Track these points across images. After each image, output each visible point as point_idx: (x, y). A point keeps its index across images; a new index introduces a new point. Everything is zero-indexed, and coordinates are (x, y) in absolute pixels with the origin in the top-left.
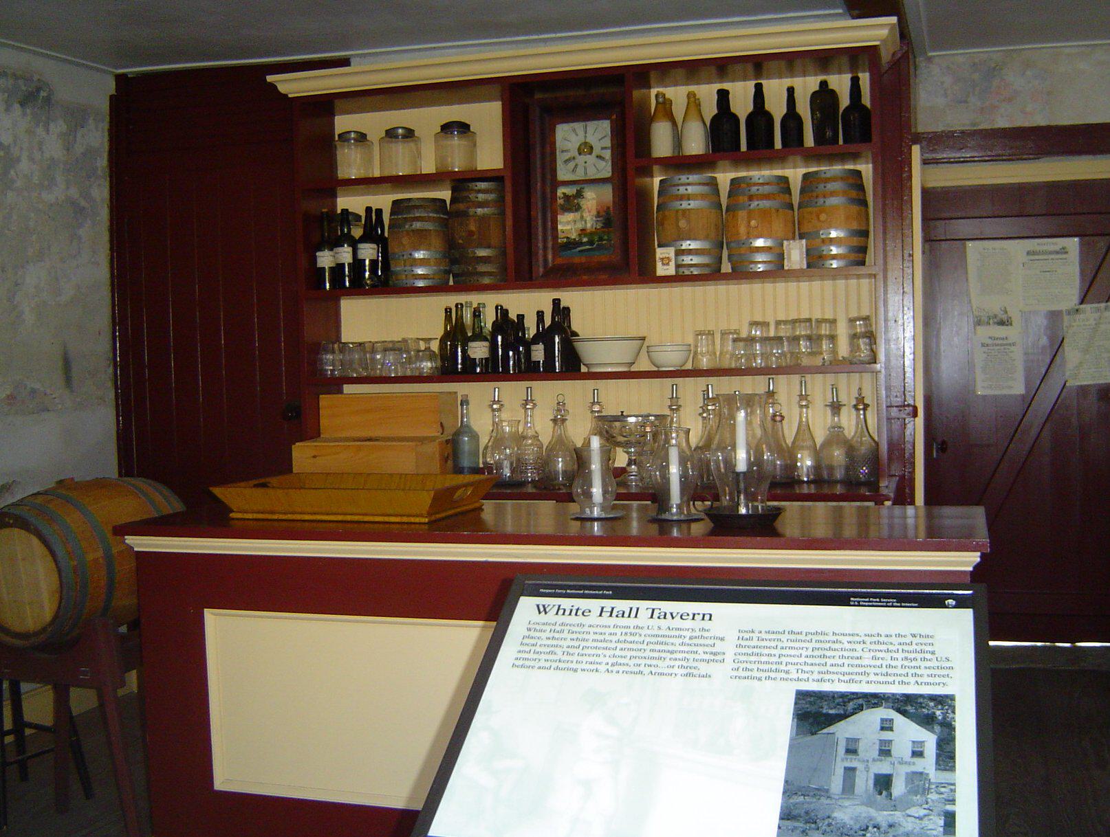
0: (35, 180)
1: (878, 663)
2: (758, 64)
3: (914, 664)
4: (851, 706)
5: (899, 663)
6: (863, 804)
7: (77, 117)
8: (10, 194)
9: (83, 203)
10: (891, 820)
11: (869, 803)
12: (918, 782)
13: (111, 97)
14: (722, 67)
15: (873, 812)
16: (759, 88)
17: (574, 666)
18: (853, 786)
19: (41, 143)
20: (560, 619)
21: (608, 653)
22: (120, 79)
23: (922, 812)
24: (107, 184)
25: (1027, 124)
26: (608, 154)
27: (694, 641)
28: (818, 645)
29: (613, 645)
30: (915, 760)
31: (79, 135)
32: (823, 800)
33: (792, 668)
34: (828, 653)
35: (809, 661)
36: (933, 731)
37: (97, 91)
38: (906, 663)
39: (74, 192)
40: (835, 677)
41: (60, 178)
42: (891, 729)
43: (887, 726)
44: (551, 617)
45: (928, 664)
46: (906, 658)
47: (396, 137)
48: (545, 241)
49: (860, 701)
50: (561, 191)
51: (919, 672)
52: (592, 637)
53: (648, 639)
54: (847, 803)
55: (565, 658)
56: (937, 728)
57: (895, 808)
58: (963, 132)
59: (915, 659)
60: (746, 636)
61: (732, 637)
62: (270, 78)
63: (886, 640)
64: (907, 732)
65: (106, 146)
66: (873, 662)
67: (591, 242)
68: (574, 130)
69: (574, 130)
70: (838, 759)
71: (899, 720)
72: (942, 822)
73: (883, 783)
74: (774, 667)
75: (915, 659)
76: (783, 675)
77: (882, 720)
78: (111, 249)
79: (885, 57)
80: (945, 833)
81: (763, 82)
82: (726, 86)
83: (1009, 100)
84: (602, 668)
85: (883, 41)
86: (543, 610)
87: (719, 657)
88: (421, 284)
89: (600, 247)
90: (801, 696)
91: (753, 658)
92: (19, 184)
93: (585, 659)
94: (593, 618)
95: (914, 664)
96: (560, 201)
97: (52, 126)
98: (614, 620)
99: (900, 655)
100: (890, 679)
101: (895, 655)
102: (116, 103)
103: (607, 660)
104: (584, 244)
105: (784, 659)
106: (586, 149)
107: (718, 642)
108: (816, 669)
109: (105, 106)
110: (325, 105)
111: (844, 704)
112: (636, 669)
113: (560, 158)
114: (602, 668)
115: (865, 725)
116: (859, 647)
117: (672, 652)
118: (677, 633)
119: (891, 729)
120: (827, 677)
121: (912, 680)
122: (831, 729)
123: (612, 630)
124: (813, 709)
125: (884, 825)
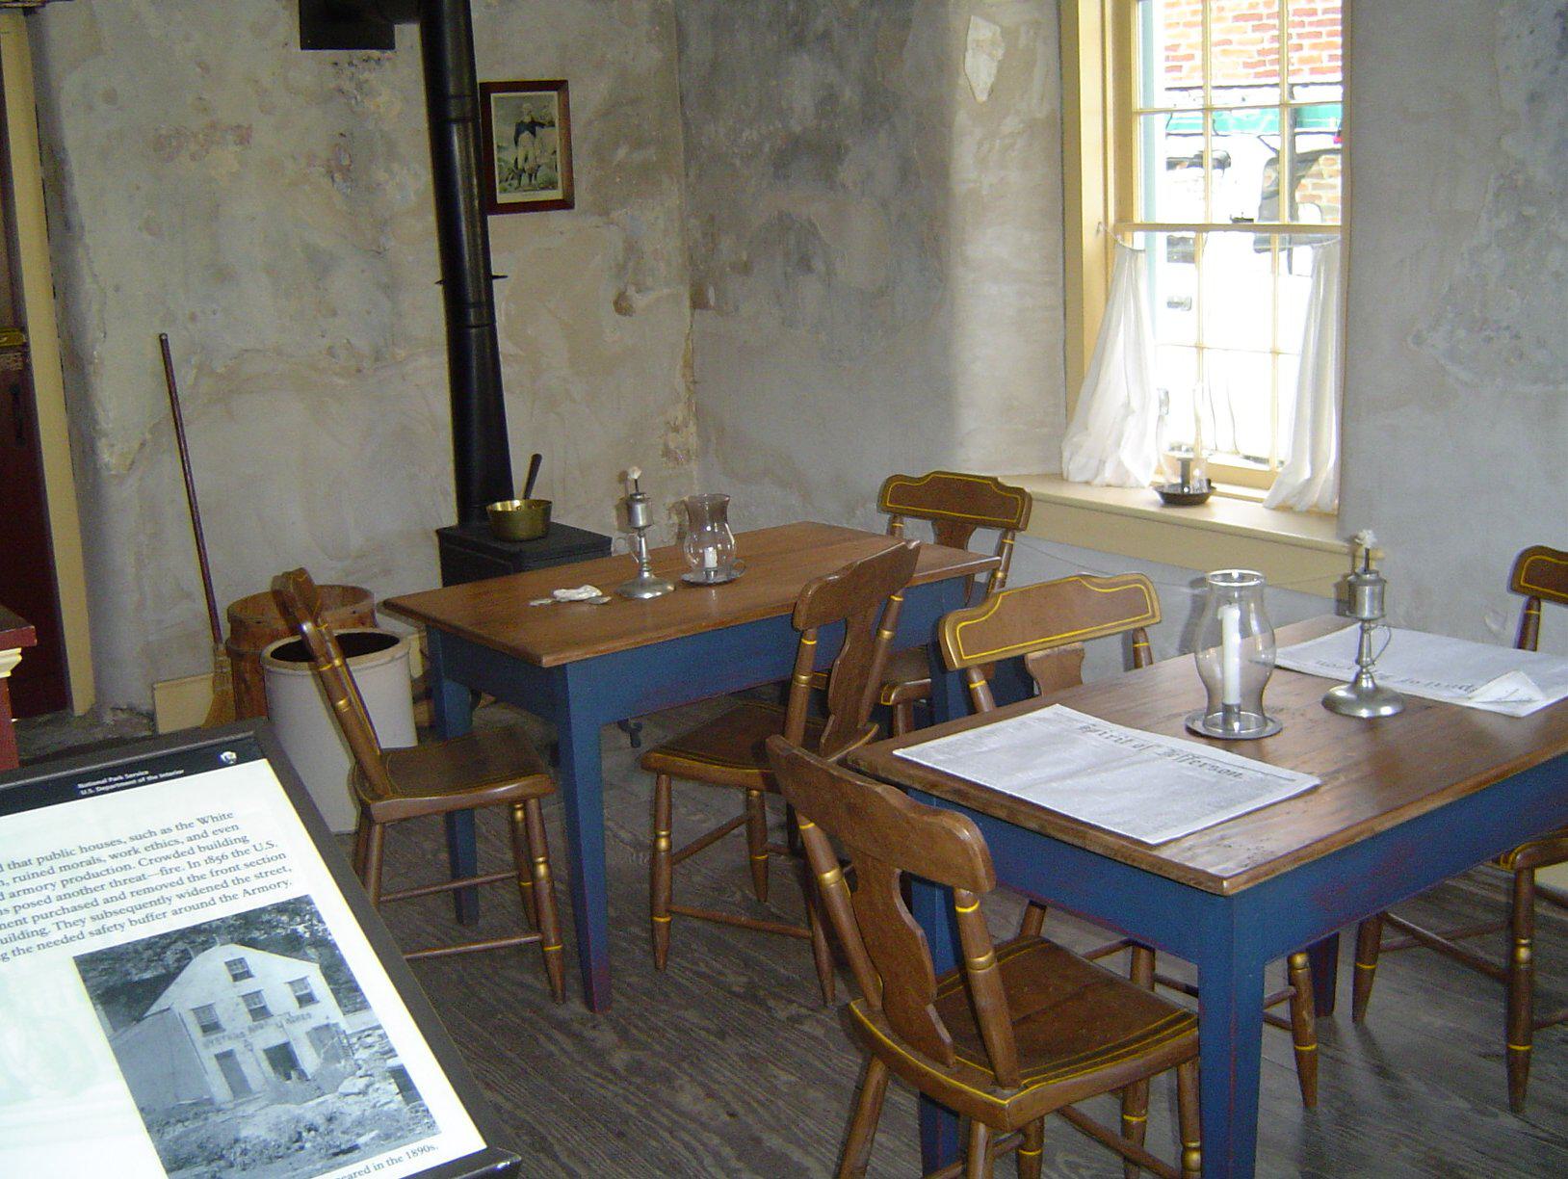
4: (170, 957)
10: (327, 1110)
11: (282, 1097)
15: (294, 1109)
23: (361, 1083)
34: (91, 883)
35: (68, 903)
36: (306, 958)
42: (247, 974)
49: (180, 945)
54: (250, 1109)
56: (311, 952)
64: (276, 973)
71: (253, 957)
72: (394, 1088)
76: (39, 940)
111: (159, 957)
116: (132, 860)
120: (109, 922)
121: (238, 890)
125: (320, 1121)
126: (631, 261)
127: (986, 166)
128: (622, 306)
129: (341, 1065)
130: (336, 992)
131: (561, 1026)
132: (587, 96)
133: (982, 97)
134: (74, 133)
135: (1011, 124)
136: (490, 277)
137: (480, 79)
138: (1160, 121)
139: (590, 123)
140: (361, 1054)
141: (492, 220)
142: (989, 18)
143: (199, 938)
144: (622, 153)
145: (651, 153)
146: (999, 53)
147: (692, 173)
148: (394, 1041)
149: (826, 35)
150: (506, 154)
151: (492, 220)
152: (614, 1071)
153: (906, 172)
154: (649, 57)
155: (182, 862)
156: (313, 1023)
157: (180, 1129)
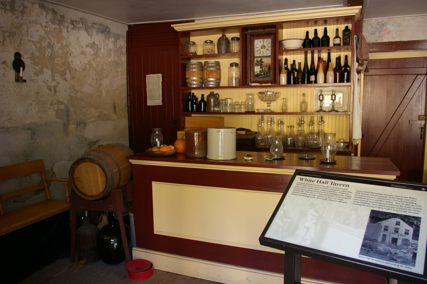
0: (106, 55)
1: (398, 205)
2: (325, 21)
3: (409, 206)
4: (387, 216)
5: (404, 206)
6: (387, 246)
7: (117, 37)
8: (98, 59)
9: (119, 62)
10: (395, 252)
11: (389, 246)
12: (406, 242)
13: (127, 31)
14: (316, 22)
15: (390, 249)
16: (326, 29)
17: (308, 196)
18: (385, 240)
19: (107, 44)
20: (306, 182)
21: (318, 193)
22: (129, 26)
23: (406, 251)
24: (126, 56)
25: (393, 41)
26: (270, 49)
27: (343, 192)
28: (380, 197)
29: (320, 191)
30: (406, 235)
31: (118, 42)
32: (375, 243)
33: (371, 203)
34: (382, 200)
35: (376, 202)
36: (412, 227)
37: (123, 30)
38: (407, 206)
39: (116, 58)
40: (384, 207)
41: (112, 54)
42: (399, 225)
43: (398, 224)
44: (303, 181)
45: (414, 207)
46: (407, 204)
47: (208, 43)
48: (251, 74)
49: (390, 215)
50: (255, 60)
51: (410, 209)
52: (314, 188)
53: (330, 190)
54: (382, 245)
55: (306, 193)
56: (414, 227)
57: (397, 249)
58: (373, 43)
59: (410, 205)
60: (358, 192)
61: (354, 192)
62: (172, 26)
63: (401, 198)
64: (404, 226)
65: (126, 46)
66: (396, 204)
67: (264, 75)
68: (260, 41)
69: (260, 41)
70: (381, 232)
71: (402, 222)
72: (412, 255)
73: (395, 241)
74: (365, 202)
75: (410, 205)
76: (368, 205)
77: (397, 222)
78: (127, 75)
79: (356, 19)
80: (413, 259)
81: (328, 27)
82: (316, 28)
83: (388, 33)
84: (316, 197)
85: (357, 14)
86: (302, 179)
87: (349, 198)
88: (194, 86)
89: (267, 76)
90: (373, 211)
91: (359, 199)
92: (101, 56)
93: (311, 194)
94: (315, 183)
95: (409, 206)
96: (255, 62)
97: (110, 39)
98: (321, 184)
99: (405, 203)
100: (401, 210)
101: (403, 203)
102: (128, 32)
103: (317, 195)
104: (262, 75)
105: (369, 200)
106: (263, 47)
107: (350, 193)
108: (378, 204)
109: (125, 34)
110: (187, 34)
111: (386, 215)
112: (325, 198)
113: (256, 49)
114: (316, 197)
115: (391, 223)
116: (392, 199)
117: (336, 195)
118: (338, 189)
119: (399, 225)
120: (381, 207)
121: (408, 211)
122: (380, 222)
123: (320, 187)
124: (376, 216)
125: (393, 253)
129: (405, 247)
148: (419, 248)
157: (369, 241)
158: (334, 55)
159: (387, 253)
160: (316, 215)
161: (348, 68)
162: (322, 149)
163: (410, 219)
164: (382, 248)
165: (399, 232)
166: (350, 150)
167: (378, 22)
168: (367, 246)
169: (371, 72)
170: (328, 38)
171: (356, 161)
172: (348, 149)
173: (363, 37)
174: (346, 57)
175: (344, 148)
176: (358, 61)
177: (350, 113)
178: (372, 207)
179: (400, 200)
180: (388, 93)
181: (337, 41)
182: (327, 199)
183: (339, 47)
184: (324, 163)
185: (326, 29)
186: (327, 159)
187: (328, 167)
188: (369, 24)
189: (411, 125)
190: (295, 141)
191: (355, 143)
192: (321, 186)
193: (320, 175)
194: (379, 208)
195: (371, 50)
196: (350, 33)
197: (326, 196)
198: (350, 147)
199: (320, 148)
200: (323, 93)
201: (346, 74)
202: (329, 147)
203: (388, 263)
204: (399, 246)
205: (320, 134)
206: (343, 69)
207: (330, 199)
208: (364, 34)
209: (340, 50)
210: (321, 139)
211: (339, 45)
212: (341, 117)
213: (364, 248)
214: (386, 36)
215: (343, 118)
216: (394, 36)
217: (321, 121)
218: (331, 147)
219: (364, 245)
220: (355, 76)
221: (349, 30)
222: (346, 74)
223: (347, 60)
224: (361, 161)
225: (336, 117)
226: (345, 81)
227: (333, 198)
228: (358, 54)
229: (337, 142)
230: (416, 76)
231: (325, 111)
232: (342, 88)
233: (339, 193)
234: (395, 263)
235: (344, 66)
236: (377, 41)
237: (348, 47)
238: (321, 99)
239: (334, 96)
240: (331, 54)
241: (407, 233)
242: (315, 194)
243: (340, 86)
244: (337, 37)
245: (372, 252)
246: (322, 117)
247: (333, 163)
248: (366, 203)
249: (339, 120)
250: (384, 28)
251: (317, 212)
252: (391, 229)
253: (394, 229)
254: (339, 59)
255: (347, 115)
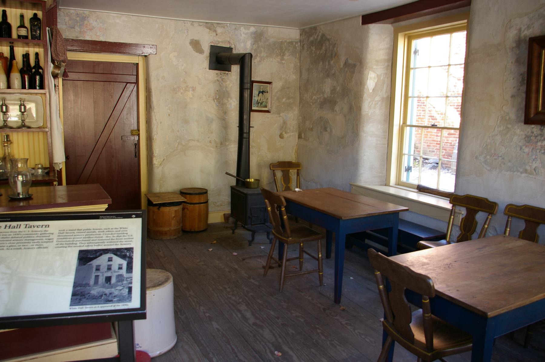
4: (98, 254)
6: (101, 287)
10: (110, 292)
11: (103, 287)
12: (120, 278)
15: (104, 290)
23: (121, 288)
25: (97, 40)
29: (10, 239)
33: (78, 242)
34: (91, 236)
35: (84, 239)
36: (125, 260)
40: (93, 244)
42: (111, 261)
45: (125, 237)
49: (101, 252)
53: (24, 236)
54: (95, 288)
56: (127, 259)
57: (112, 287)
58: (73, 40)
60: (62, 232)
61: (56, 232)
64: (117, 261)
71: (115, 258)
72: (127, 290)
76: (75, 245)
83: (91, 30)
91: (64, 240)
98: (11, 230)
103: (6, 245)
105: (75, 240)
107: (51, 235)
111: (96, 253)
112: (19, 247)
114: (5, 248)
115: (103, 260)
116: (102, 233)
117: (33, 240)
119: (111, 261)
120: (90, 244)
121: (119, 243)
125: (108, 293)
126: (284, 127)
127: (371, 108)
128: (281, 136)
129: (120, 283)
130: (127, 268)
131: (239, 311)
132: (277, 85)
133: (371, 91)
134: (154, 85)
135: (377, 98)
136: (250, 127)
137: (252, 79)
138: (416, 100)
139: (277, 92)
140: (125, 282)
141: (252, 113)
142: (374, 72)
143: (106, 251)
144: (284, 100)
145: (291, 101)
146: (376, 80)
147: (301, 106)
148: (134, 281)
149: (334, 74)
150: (255, 98)
151: (252, 113)
152: (249, 324)
153: (351, 108)
154: (293, 77)
155: (112, 236)
156: (119, 273)
157: (79, 288)
158: (20, 51)
159: (102, 296)
160: (8, 271)
161: (41, 71)
162: (10, 181)
163: (122, 252)
164: (95, 291)
165: (112, 269)
166: (52, 178)
167: (77, 14)
168: (78, 295)
169: (71, 76)
170: (9, 26)
171: (61, 191)
172: (49, 177)
173: (58, 32)
174: (37, 54)
175: (43, 176)
176: (53, 61)
177: (47, 130)
178: (80, 246)
179: (110, 233)
180: (95, 103)
181: (23, 32)
182: (21, 248)
183: (25, 40)
184: (14, 199)
185: (4, 12)
186: (19, 194)
187: (22, 204)
188: (67, 14)
189: (124, 141)
190: (7, 154)
191: (57, 168)
192: (11, 232)
193: (8, 218)
194: (88, 246)
195: (69, 48)
196: (40, 23)
197: (19, 244)
198: (51, 174)
199: (7, 179)
200: (7, 102)
201: (38, 78)
202: (20, 178)
203: (104, 307)
204: (114, 284)
205: (7, 159)
206: (34, 70)
207: (26, 247)
208: (59, 26)
209: (27, 44)
210: (9, 165)
211: (26, 37)
212: (36, 135)
213: (75, 297)
214: (88, 33)
215: (39, 135)
216: (98, 34)
217: (7, 141)
218: (23, 177)
219: (74, 294)
220: (50, 81)
221: (39, 19)
222: (38, 78)
223: (38, 59)
224: (68, 191)
225: (33, 135)
226: (37, 88)
227: (29, 245)
228: (53, 52)
229: (33, 169)
230: (125, 84)
231: (11, 128)
232: (34, 97)
233: (37, 237)
234: (111, 305)
235: (34, 67)
236: (77, 37)
237: (39, 42)
238: (4, 110)
239: (23, 107)
240: (16, 49)
241: (120, 268)
242: (4, 245)
243: (31, 94)
244: (22, 26)
245: (84, 300)
246: (8, 136)
247: (28, 198)
248: (72, 244)
249: (34, 139)
250: (86, 22)
251: (8, 268)
252: (104, 268)
253: (106, 267)
254: (26, 56)
255: (43, 132)
